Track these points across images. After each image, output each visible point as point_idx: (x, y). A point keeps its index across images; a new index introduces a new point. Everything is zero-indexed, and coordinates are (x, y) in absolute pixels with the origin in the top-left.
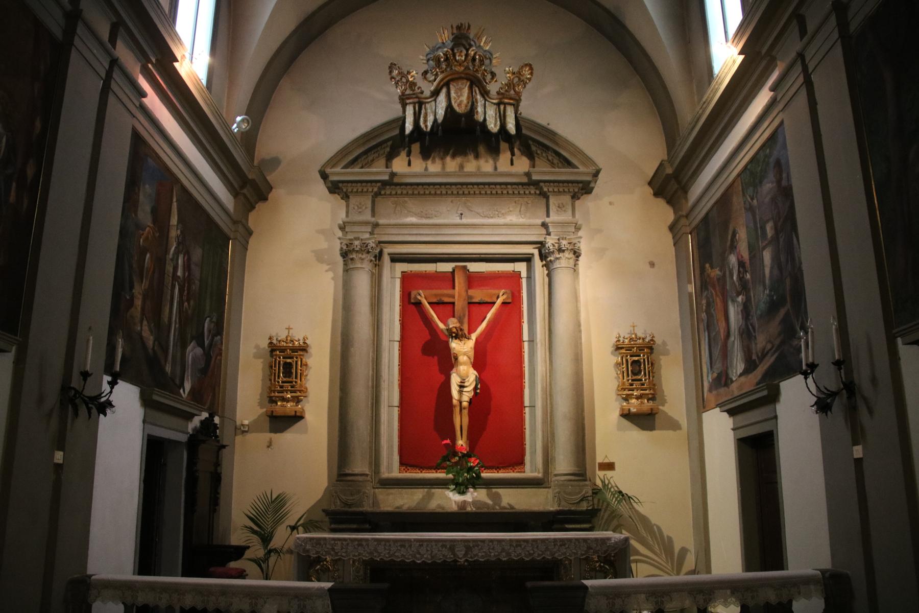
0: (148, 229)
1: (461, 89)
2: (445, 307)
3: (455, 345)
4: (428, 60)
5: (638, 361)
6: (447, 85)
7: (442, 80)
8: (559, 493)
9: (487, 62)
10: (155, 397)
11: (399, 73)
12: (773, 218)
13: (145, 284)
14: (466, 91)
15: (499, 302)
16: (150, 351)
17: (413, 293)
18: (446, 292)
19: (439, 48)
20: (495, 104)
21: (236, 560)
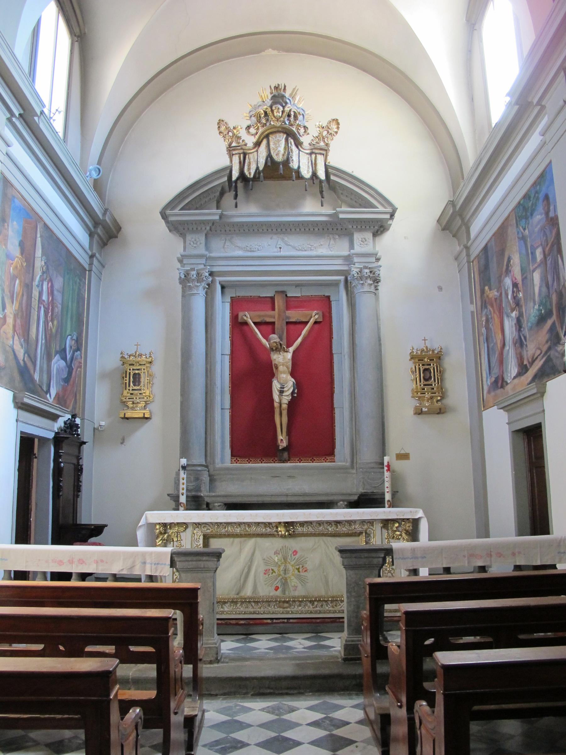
1: (279, 141)
2: (267, 326)
4: (251, 116)
6: (267, 137)
7: (263, 133)
8: (363, 478)
9: (300, 117)
10: (26, 400)
11: (227, 128)
12: (542, 245)
13: (16, 305)
14: (283, 141)
15: (312, 321)
16: (22, 363)
17: (241, 314)
19: (260, 106)
20: (307, 154)
21: (96, 536)
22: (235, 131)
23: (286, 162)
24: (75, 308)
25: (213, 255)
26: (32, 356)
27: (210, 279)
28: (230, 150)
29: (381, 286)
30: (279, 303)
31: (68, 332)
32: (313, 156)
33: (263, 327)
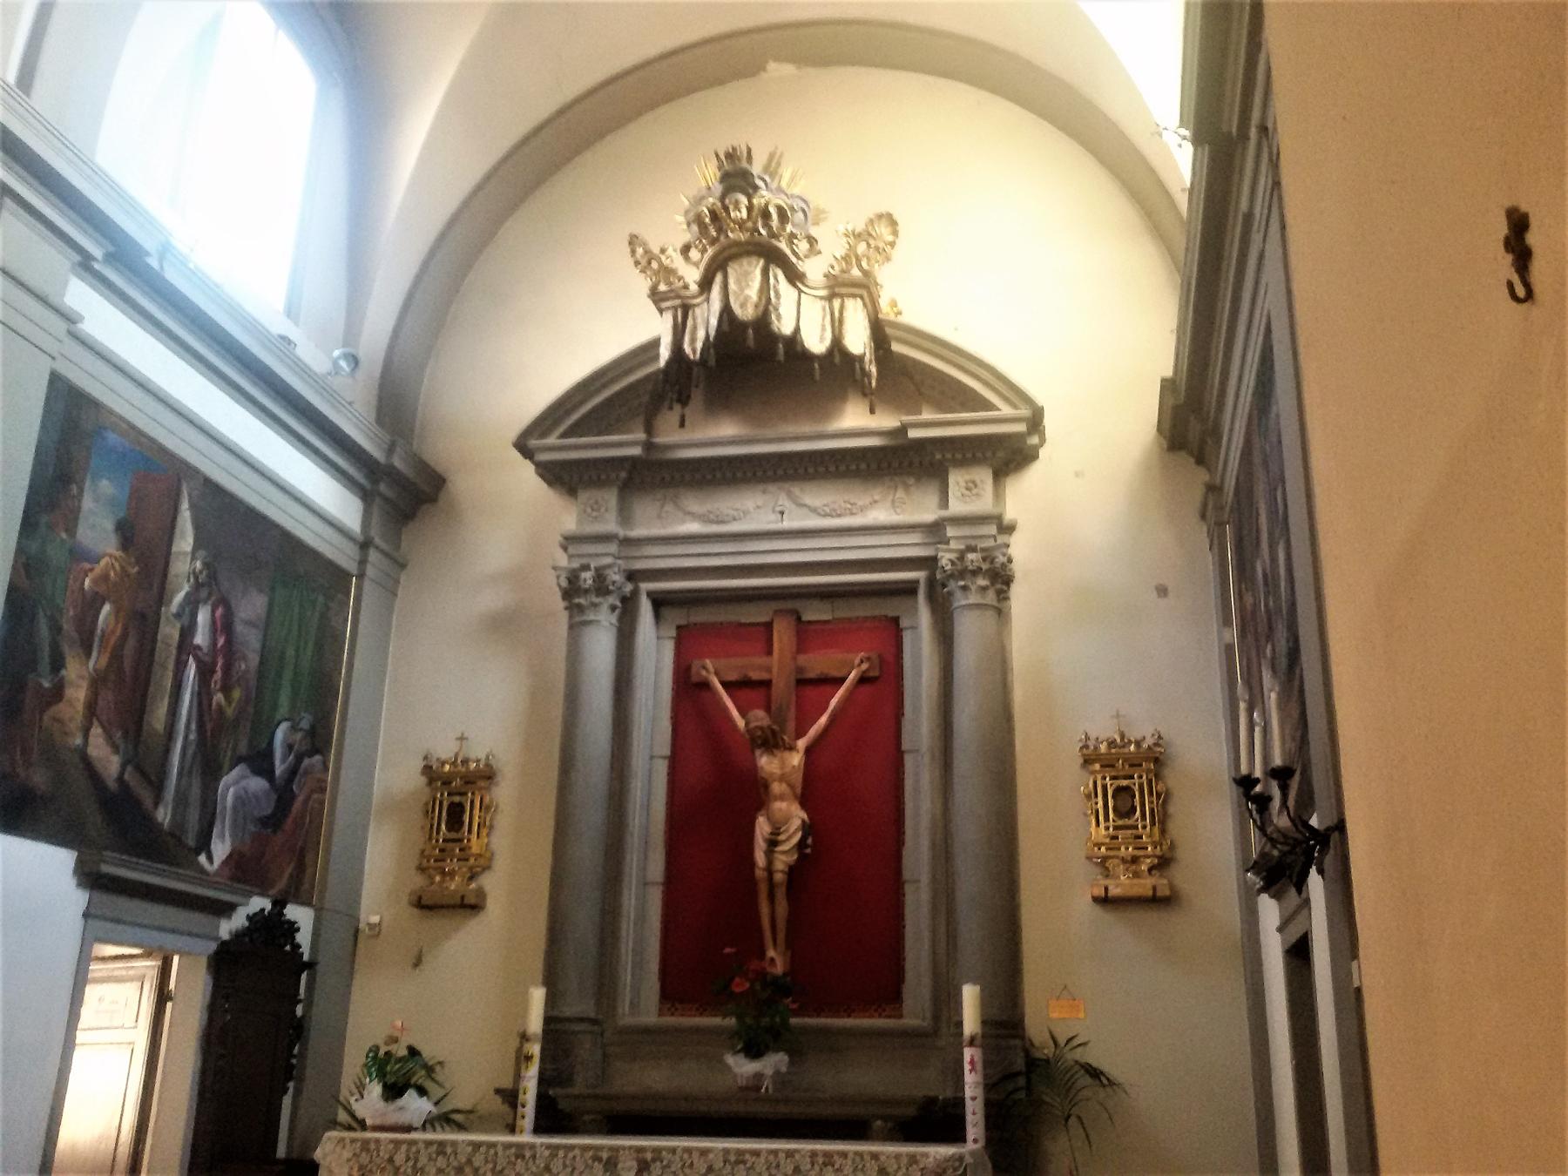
1: (747, 274)
3: (767, 763)
5: (1127, 789)
10: (106, 869)
11: (647, 252)
13: (98, 660)
14: (758, 273)
17: (696, 665)
20: (822, 298)
22: (663, 258)
25: (638, 532)
27: (629, 588)
29: (1017, 592)
30: (783, 635)
31: (283, 710)
32: (837, 303)
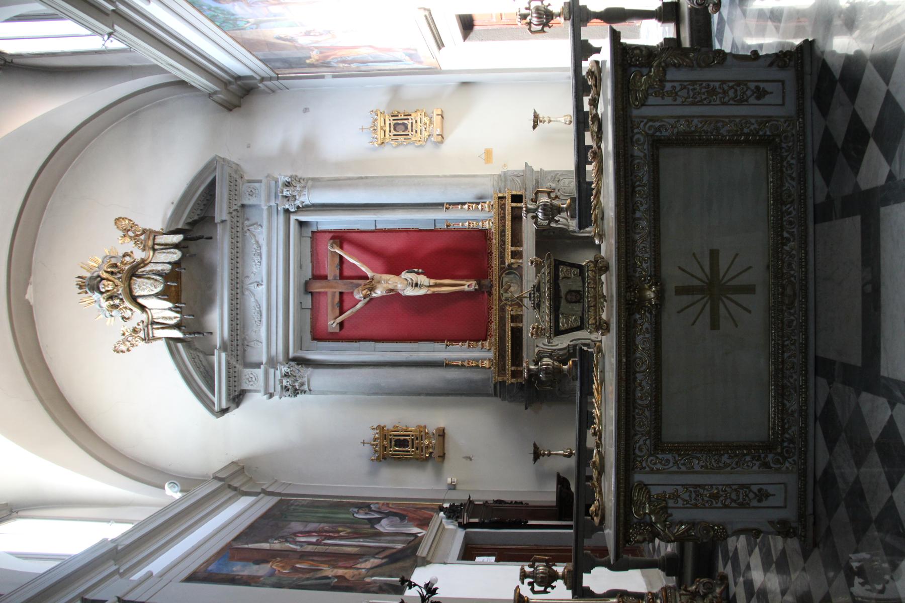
0: (274, 567)
9: (113, 261)
16: (384, 561)
18: (329, 300)
23: (166, 277)
24: (324, 510)
26: (377, 551)
28: (148, 339)
30: (317, 287)
32: (157, 247)
33: (346, 304)
